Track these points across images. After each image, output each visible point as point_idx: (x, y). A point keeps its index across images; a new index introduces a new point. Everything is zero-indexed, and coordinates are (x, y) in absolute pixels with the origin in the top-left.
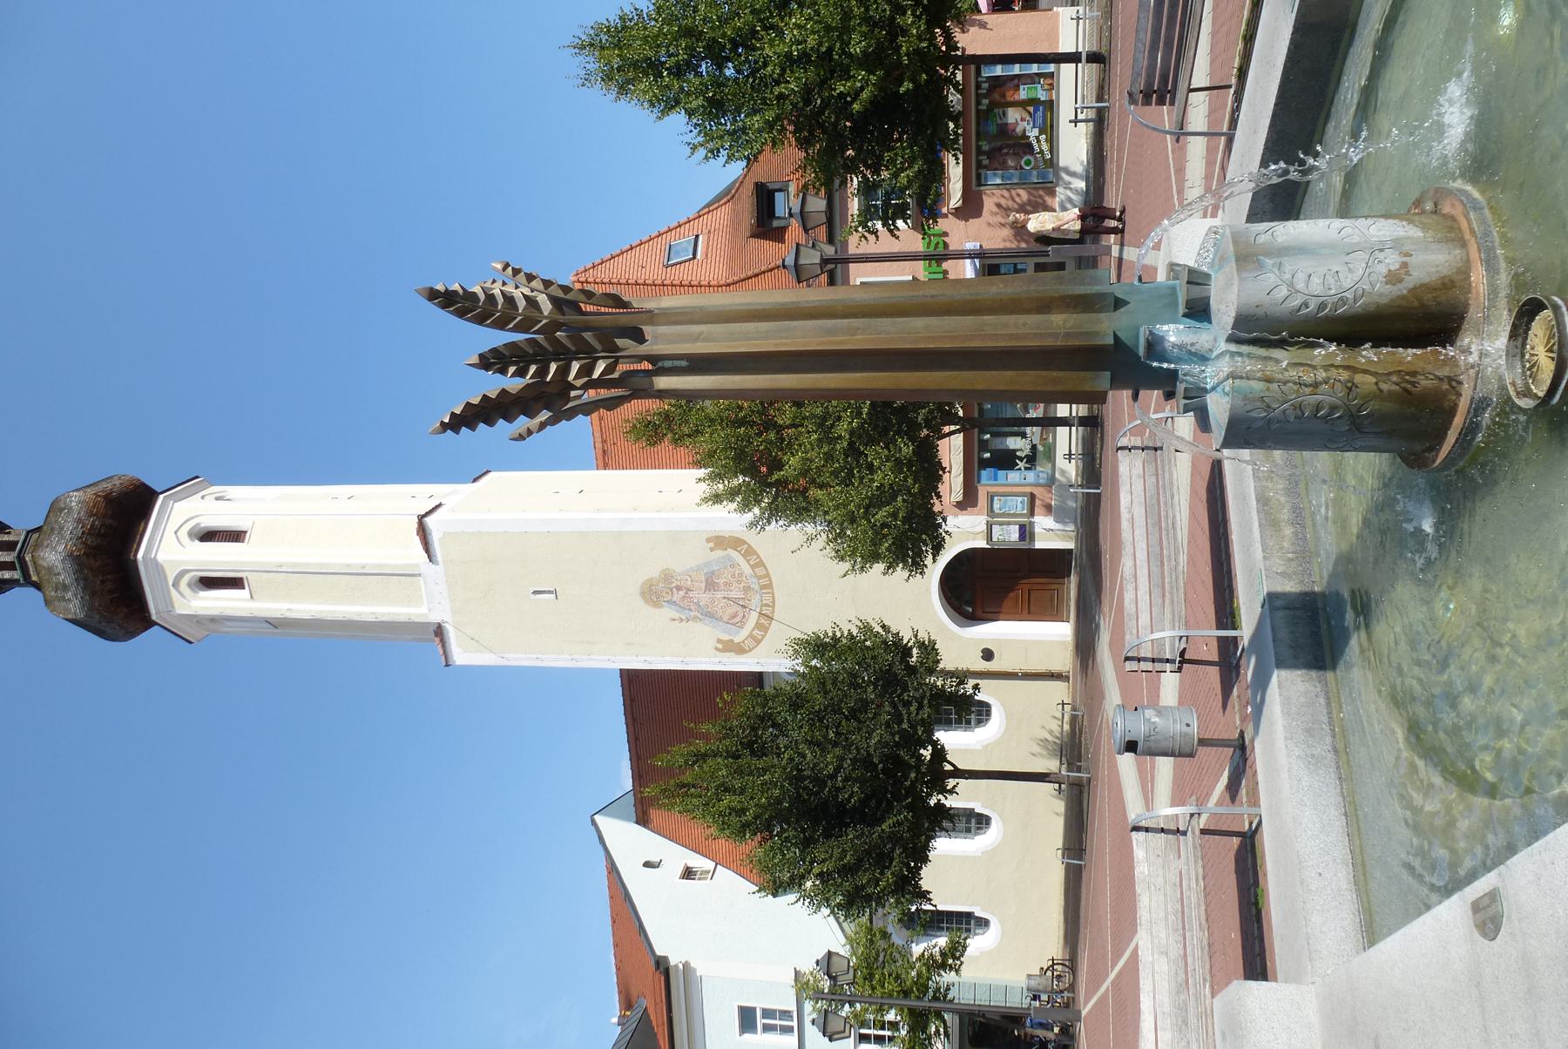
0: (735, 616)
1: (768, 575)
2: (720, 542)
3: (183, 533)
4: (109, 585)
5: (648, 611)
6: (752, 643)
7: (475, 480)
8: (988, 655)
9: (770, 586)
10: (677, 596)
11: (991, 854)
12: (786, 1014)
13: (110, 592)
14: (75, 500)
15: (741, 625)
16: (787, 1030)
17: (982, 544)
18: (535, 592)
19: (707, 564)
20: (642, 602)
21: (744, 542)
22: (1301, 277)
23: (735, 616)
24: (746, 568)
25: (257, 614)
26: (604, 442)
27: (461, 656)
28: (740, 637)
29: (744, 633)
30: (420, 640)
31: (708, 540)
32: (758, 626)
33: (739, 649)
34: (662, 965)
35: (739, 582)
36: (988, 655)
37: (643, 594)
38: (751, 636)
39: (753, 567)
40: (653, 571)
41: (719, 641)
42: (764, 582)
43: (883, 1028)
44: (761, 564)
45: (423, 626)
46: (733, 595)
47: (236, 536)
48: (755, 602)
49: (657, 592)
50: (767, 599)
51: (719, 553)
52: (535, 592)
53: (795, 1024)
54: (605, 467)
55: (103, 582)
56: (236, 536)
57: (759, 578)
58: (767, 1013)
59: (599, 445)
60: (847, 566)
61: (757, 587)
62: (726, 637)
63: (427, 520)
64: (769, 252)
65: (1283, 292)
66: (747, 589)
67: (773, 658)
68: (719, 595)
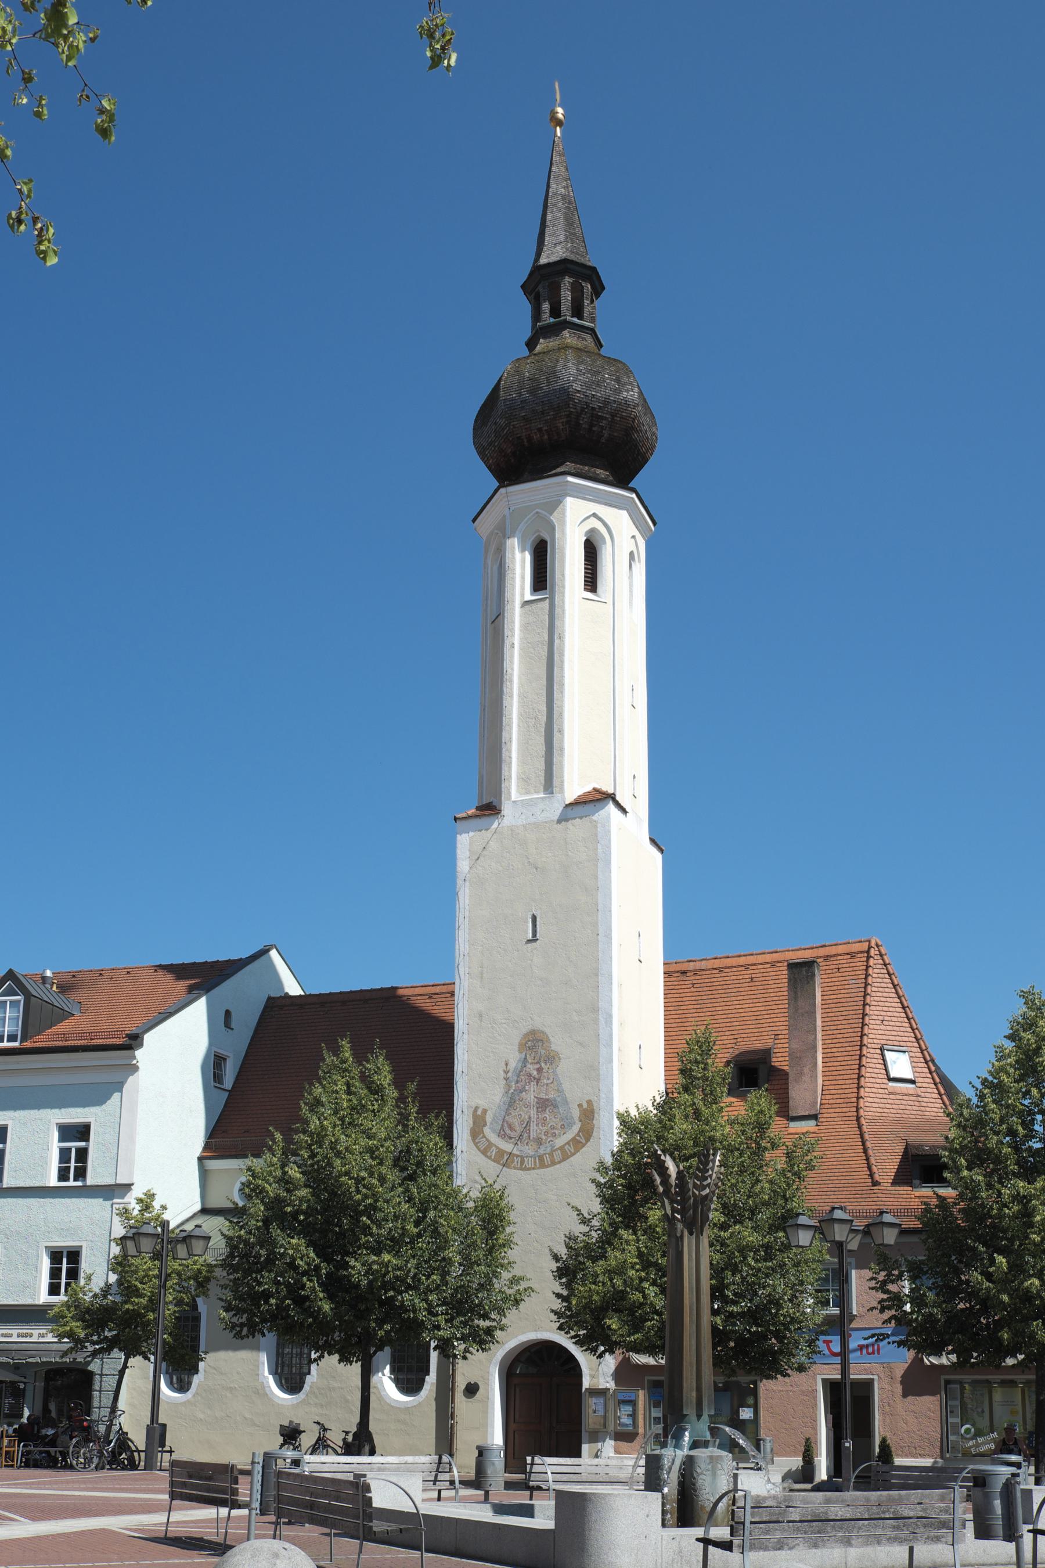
0: (511, 1128)
1: (553, 1163)
2: (588, 1114)
3: (594, 523)
4: (536, 437)
5: (516, 1038)
6: (483, 1145)
7: (653, 841)
8: (472, 1390)
9: (543, 1165)
10: (532, 1069)
11: (262, 1392)
12: (81, 1173)
13: (529, 438)
14: (631, 395)
15: (502, 1135)
16: (63, 1175)
17: (586, 1383)
18: (534, 919)
19: (566, 1102)
20: (524, 1031)
21: (588, 1140)
22: (704, 1477)
23: (511, 1128)
24: (559, 1142)
25: (507, 607)
26: (695, 973)
27: (465, 842)
28: (490, 1134)
29: (494, 1138)
30: (481, 783)
31: (589, 1102)
32: (501, 1152)
33: (476, 1132)
34: (134, 1041)
35: (546, 1133)
36: (472, 1390)
37: (533, 1032)
38: (490, 1145)
39: (562, 1148)
40: (558, 1042)
41: (485, 1111)
42: (547, 1159)
43: (60, 1269)
44: (565, 1157)
45: (498, 793)
46: (533, 1127)
47: (591, 582)
48: (529, 1150)
49: (534, 1043)
50: (529, 1162)
51: (576, 1113)
52: (534, 919)
53: (71, 1183)
54: (668, 974)
55: (540, 430)
56: (591, 582)
57: (551, 1154)
58: (82, 1155)
59: (691, 966)
60: (563, 1252)
61: (541, 1151)
62: (489, 1118)
63: (611, 806)
64: (887, 1166)
65: (699, 1470)
66: (539, 1142)
67: (469, 1169)
68: (533, 1112)
